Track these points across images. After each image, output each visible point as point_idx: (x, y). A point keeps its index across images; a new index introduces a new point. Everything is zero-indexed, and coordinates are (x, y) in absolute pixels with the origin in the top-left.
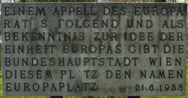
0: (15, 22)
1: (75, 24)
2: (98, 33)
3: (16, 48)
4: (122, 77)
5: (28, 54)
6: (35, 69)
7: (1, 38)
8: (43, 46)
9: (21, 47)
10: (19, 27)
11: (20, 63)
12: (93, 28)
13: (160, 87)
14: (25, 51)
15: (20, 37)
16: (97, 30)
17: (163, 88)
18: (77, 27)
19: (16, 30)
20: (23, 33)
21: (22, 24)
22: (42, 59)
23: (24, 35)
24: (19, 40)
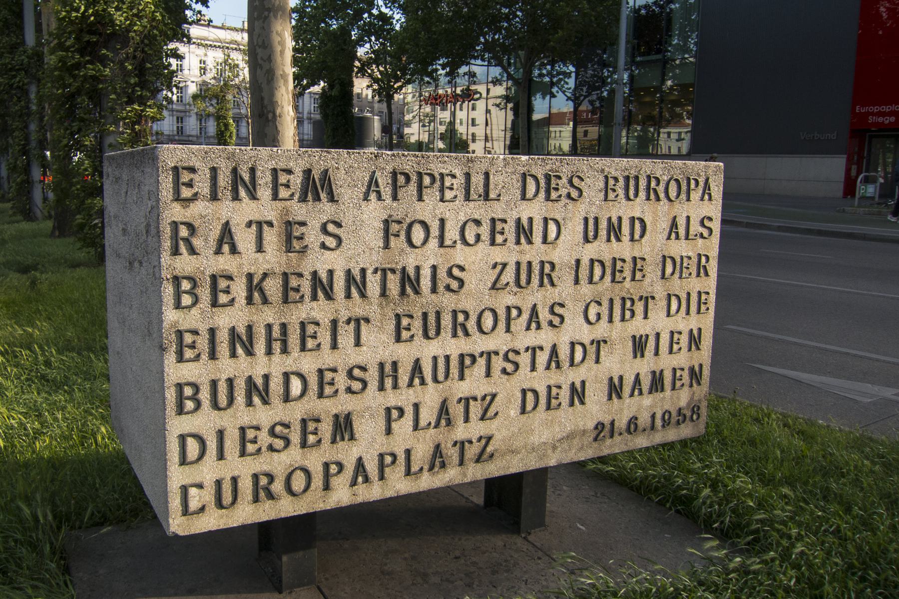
0: (216, 233)
1: (437, 234)
2: (505, 265)
3: (223, 337)
4: (563, 404)
5: (270, 360)
6: (295, 413)
7: (881, 161)
8: (326, 322)
9: (242, 330)
10: (234, 250)
11: (240, 399)
12: (175, 204)
13: (220, 25)
14: (260, 347)
15: (239, 289)
16: (498, 255)
17: (659, 422)
18: (442, 245)
19: (225, 262)
20: (250, 276)
21: (245, 239)
22: (321, 372)
23: (255, 281)
24: (236, 305)
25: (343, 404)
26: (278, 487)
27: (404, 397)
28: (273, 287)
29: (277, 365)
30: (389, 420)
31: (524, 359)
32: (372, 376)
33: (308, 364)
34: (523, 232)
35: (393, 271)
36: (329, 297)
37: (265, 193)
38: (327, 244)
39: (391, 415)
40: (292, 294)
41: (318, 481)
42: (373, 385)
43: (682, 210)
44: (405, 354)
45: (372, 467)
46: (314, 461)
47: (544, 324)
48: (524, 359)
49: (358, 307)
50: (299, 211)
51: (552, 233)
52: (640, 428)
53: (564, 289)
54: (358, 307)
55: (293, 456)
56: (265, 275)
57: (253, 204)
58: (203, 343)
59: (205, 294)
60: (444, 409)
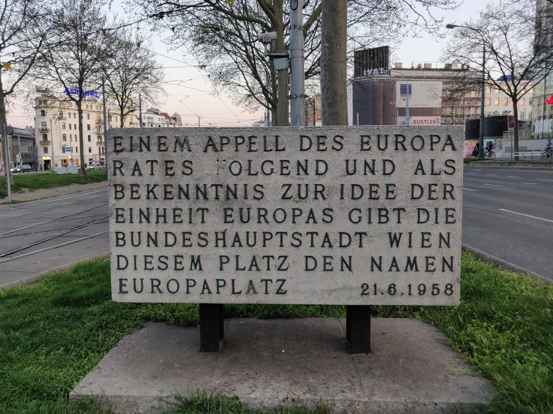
3: (136, 213)
14: (153, 219)
15: (143, 192)
21: (145, 169)
23: (150, 188)
25: (196, 251)
26: (163, 287)
27: (231, 252)
28: (159, 191)
29: (161, 229)
30: (222, 263)
31: (306, 240)
32: (211, 238)
33: (178, 230)
34: (302, 167)
35: (221, 186)
36: (187, 196)
37: (154, 148)
38: (185, 172)
39: (223, 261)
40: (327, 266)
41: (183, 288)
42: (212, 243)
43: (425, 157)
44: (232, 229)
45: (213, 287)
46: (182, 277)
47: (319, 221)
48: (306, 240)
49: (202, 204)
50: (172, 155)
51: (389, 169)
52: (398, 292)
53: (334, 201)
54: (202, 204)
55: (170, 273)
56: (155, 186)
57: (149, 153)
58: (127, 214)
59: (128, 193)
60: (254, 261)
